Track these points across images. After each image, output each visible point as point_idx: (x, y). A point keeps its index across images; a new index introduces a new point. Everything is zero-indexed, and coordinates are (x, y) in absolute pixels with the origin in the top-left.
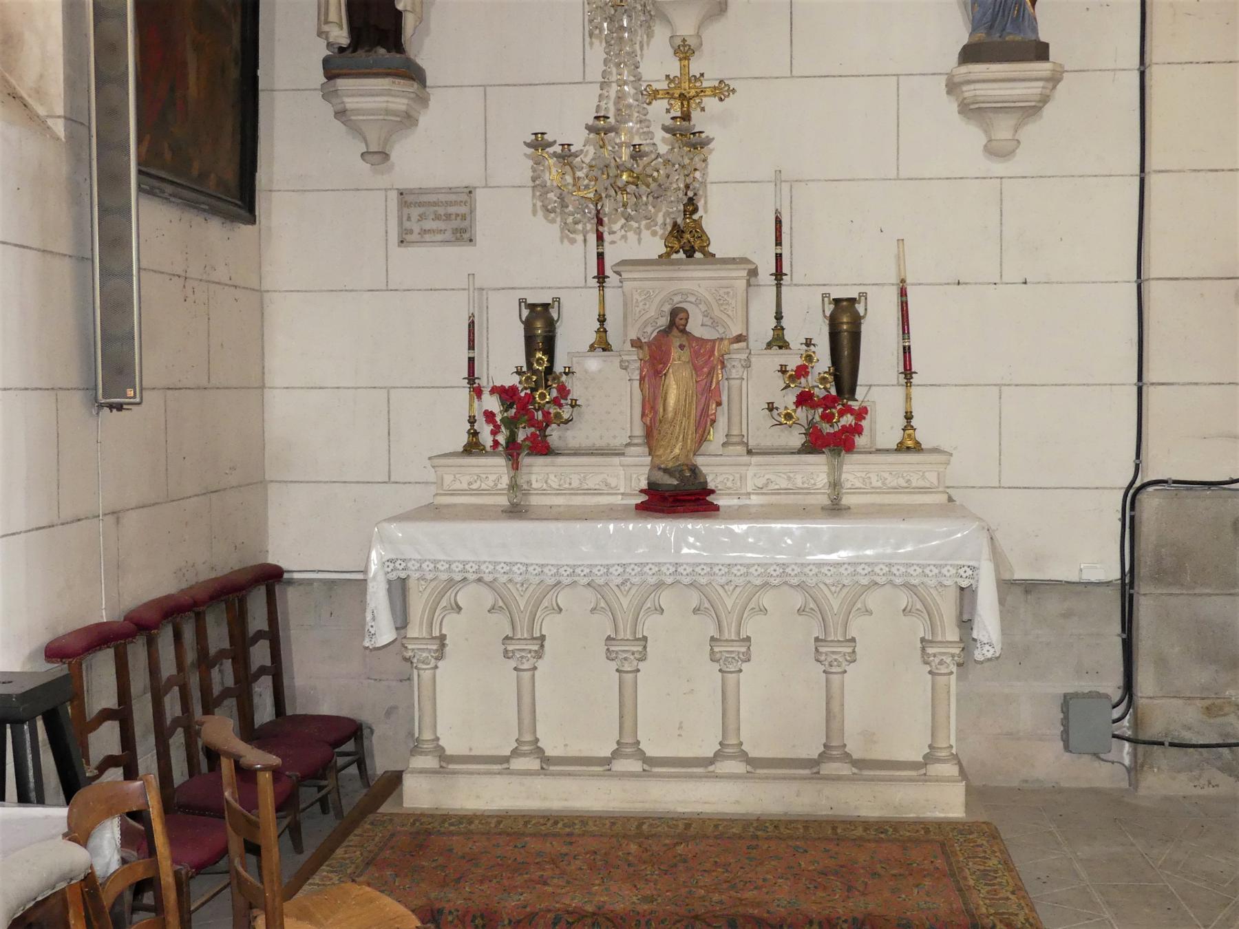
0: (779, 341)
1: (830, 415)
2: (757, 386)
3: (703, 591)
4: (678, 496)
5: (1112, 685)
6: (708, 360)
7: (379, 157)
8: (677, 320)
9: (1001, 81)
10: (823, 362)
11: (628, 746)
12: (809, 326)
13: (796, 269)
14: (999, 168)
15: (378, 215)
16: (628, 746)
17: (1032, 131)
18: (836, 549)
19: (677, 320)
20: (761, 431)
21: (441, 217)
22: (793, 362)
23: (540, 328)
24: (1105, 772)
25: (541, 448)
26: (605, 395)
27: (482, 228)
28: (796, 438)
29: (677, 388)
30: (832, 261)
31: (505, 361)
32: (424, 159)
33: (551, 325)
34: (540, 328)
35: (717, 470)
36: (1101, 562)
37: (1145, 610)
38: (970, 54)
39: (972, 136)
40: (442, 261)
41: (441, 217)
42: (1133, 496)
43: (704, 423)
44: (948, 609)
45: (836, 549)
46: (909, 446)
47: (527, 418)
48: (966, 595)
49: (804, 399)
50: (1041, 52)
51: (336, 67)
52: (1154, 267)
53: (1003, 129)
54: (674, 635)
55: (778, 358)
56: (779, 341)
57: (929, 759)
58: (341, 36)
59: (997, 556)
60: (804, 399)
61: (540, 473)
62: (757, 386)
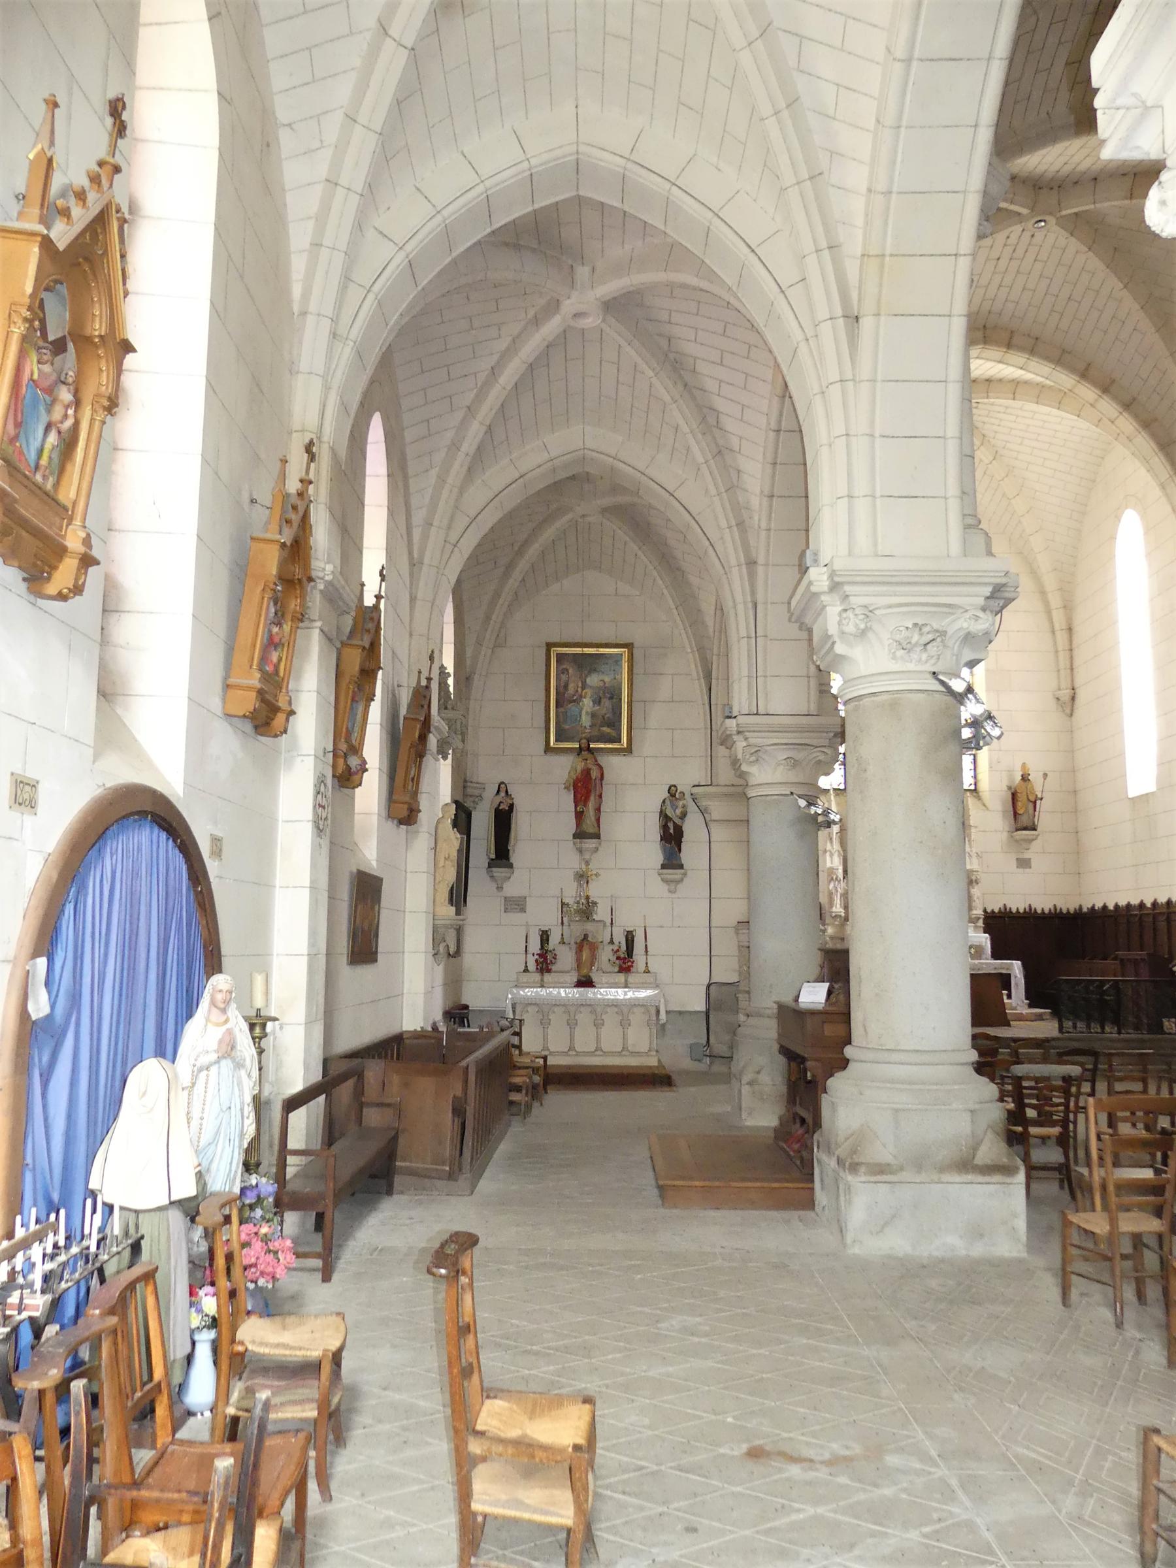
0: (612, 942)
1: (625, 963)
2: (606, 955)
3: (591, 1006)
4: (585, 982)
5: (704, 1042)
6: (594, 948)
7: (500, 888)
8: (586, 936)
9: (674, 874)
10: (624, 948)
11: (571, 1048)
12: (620, 938)
13: (617, 922)
14: (674, 896)
15: (498, 904)
16: (571, 1048)
17: (680, 886)
18: (619, 994)
19: (586, 936)
20: (605, 965)
21: (516, 905)
22: (616, 948)
23: (545, 937)
24: (703, 1066)
25: (549, 971)
26: (566, 958)
27: (528, 909)
28: (617, 969)
29: (585, 954)
30: (628, 919)
31: (535, 946)
32: (513, 888)
33: (548, 936)
34: (545, 937)
35: (595, 977)
36: (700, 1006)
37: (711, 1017)
38: (664, 867)
39: (666, 887)
40: (516, 917)
41: (516, 905)
42: (709, 986)
43: (592, 964)
44: (653, 1011)
45: (619, 994)
46: (647, 971)
47: (545, 963)
48: (658, 1012)
49: (618, 958)
50: (681, 867)
51: (492, 864)
52: (713, 924)
53: (672, 886)
54: (584, 1018)
55: (611, 947)
56: (612, 942)
57: (650, 1050)
58: (493, 856)
59: (666, 1001)
60: (618, 958)
61: (548, 977)
62: (606, 955)
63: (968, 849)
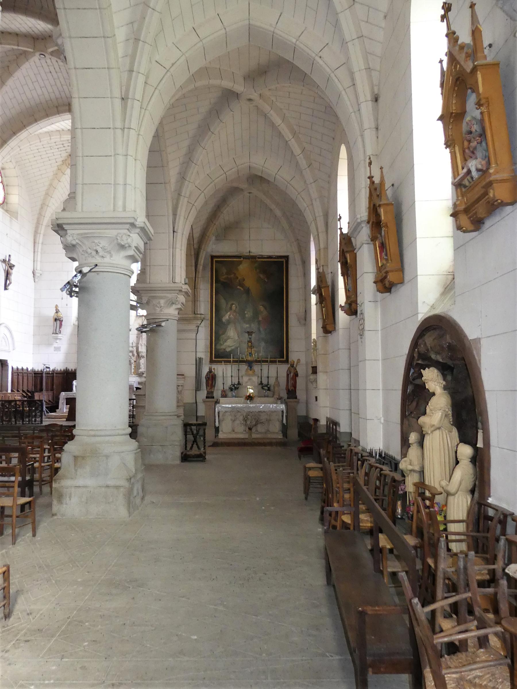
63: (140, 342)
